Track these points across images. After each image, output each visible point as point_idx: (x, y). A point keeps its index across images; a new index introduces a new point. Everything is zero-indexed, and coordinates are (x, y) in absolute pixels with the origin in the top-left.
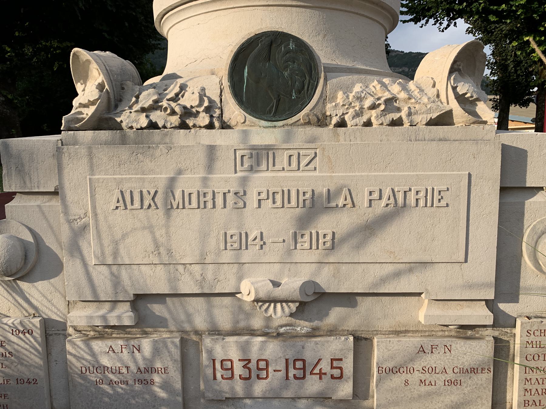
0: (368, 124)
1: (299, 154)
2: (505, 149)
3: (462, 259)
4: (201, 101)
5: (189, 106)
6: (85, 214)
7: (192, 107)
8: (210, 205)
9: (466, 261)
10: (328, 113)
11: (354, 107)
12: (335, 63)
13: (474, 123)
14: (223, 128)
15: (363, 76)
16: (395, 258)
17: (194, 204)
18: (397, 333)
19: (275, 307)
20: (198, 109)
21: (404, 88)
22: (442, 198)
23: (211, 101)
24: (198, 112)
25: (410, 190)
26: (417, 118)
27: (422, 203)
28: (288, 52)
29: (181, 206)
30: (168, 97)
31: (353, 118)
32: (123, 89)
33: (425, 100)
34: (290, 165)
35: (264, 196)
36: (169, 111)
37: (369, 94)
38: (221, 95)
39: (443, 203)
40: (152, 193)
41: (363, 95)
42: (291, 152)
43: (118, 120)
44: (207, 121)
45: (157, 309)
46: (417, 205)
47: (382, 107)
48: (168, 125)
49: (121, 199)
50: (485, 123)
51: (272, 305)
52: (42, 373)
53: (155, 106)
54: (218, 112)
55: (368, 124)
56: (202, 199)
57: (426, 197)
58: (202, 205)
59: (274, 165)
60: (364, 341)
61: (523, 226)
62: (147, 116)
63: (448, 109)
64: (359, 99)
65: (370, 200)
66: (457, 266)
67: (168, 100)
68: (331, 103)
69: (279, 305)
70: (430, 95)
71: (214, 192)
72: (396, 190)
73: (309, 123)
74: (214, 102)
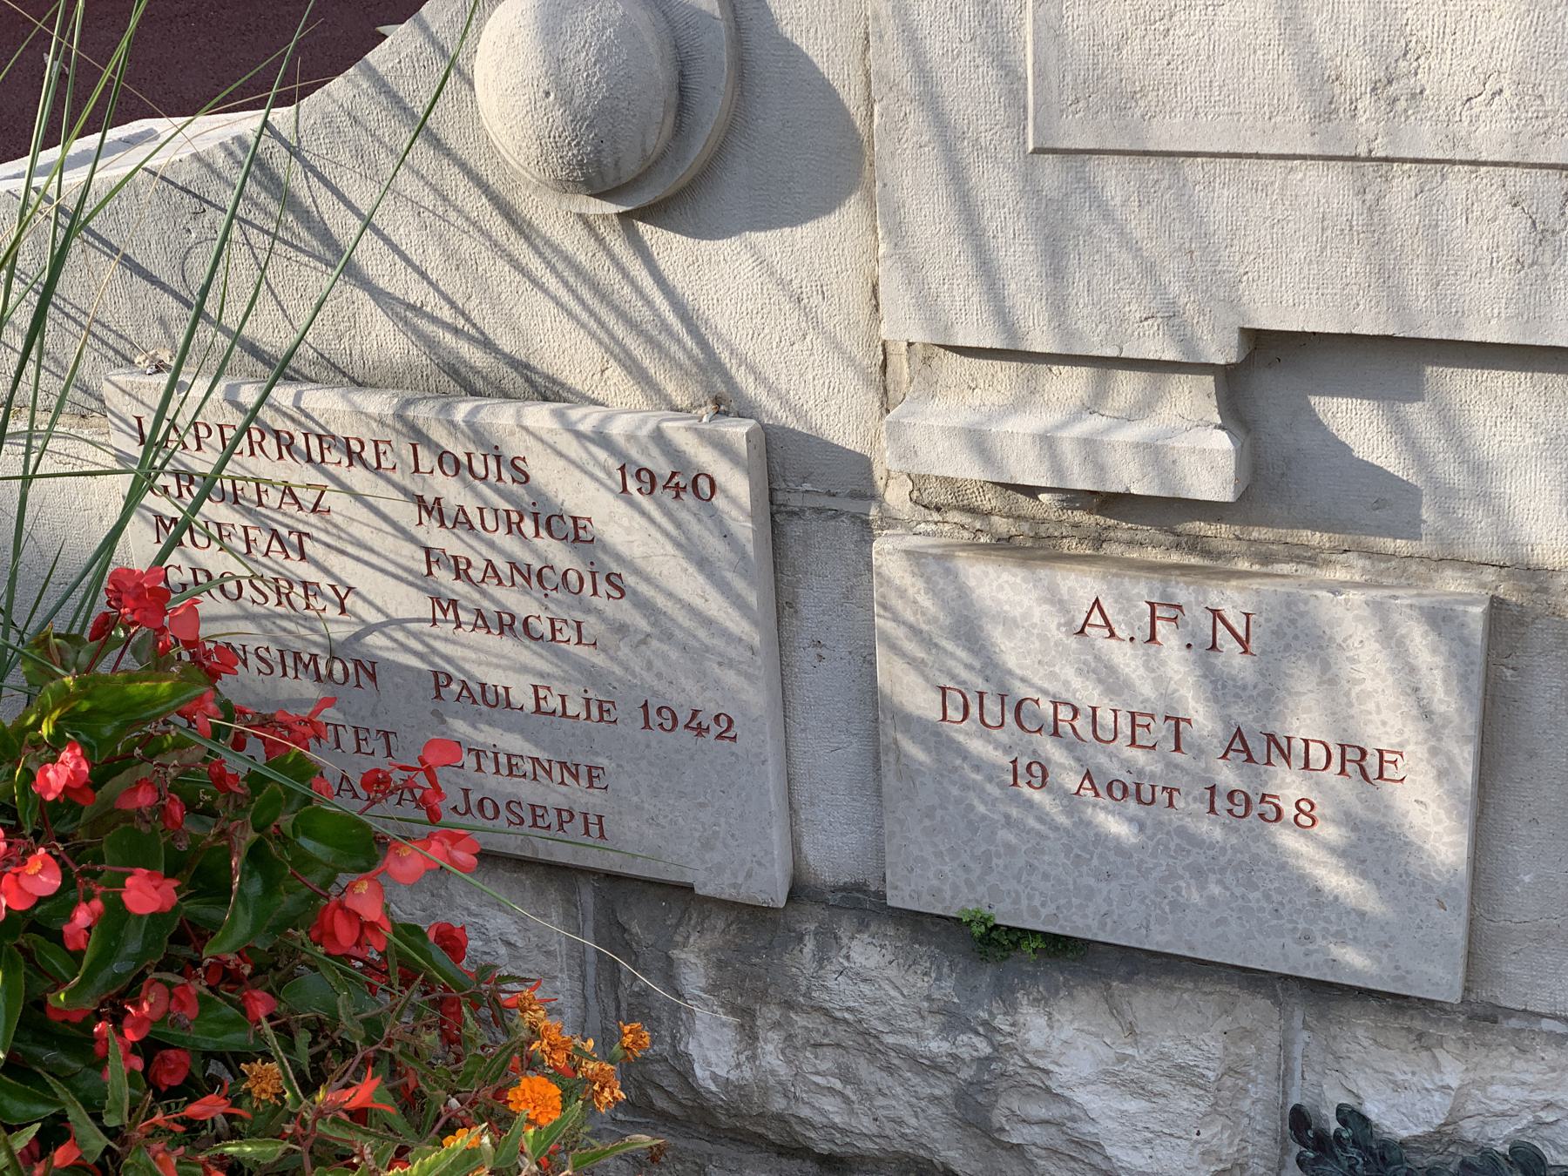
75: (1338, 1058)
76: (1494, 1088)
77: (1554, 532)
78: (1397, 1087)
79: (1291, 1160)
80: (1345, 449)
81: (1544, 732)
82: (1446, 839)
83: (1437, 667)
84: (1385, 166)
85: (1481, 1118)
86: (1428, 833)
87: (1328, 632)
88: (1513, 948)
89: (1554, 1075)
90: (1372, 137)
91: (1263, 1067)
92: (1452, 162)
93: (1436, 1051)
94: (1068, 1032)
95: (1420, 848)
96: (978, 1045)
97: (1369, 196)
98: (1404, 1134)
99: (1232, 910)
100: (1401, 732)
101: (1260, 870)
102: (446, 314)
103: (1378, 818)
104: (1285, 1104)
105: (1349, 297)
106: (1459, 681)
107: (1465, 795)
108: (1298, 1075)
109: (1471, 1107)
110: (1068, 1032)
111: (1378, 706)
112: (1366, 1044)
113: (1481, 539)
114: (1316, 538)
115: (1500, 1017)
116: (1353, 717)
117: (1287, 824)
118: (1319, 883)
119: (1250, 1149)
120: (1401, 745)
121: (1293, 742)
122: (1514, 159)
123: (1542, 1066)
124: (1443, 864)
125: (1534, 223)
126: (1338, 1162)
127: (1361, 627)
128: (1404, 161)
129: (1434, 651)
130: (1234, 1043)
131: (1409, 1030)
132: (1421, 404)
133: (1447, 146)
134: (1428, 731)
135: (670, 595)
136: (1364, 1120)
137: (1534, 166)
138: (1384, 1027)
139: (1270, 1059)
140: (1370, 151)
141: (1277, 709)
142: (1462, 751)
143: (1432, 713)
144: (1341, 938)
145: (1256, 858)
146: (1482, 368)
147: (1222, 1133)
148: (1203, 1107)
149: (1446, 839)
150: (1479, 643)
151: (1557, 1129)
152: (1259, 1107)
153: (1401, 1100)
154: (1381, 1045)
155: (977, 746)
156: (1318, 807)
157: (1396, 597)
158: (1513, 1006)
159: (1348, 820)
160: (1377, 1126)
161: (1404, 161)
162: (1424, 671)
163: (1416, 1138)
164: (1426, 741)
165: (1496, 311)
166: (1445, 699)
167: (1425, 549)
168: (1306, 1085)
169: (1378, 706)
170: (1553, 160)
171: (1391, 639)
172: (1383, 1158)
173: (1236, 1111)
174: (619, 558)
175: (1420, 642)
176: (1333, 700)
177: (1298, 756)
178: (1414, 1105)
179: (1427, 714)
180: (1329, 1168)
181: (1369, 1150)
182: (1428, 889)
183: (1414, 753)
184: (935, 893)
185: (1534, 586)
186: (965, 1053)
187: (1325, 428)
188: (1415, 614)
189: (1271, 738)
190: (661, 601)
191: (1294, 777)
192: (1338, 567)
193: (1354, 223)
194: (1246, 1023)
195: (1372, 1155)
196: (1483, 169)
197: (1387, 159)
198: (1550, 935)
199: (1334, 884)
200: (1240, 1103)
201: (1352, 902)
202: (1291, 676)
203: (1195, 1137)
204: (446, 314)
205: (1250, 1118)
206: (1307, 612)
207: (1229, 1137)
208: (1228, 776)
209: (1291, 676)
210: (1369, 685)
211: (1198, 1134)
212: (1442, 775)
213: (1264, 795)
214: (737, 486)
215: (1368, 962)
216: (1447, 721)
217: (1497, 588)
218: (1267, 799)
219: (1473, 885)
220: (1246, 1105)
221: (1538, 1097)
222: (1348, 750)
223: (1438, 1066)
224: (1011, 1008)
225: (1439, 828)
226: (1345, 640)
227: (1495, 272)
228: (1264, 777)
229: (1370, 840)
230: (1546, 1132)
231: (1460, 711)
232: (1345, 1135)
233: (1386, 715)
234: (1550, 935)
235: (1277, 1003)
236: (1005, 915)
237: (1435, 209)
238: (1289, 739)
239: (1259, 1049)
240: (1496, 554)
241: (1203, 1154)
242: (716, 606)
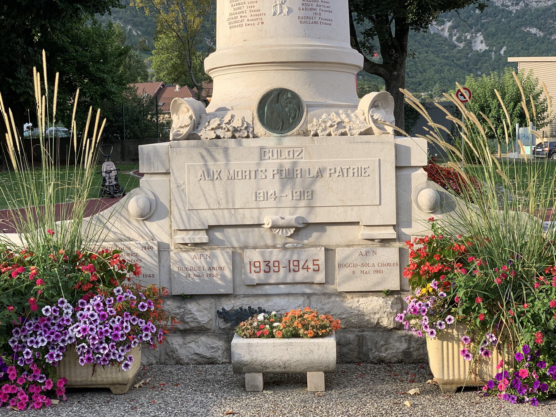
0: (329, 135)
1: (294, 150)
2: (396, 146)
3: (378, 203)
4: (243, 124)
5: (236, 127)
6: (184, 183)
7: (238, 127)
8: (248, 177)
9: (380, 204)
10: (309, 129)
11: (322, 126)
12: (315, 101)
13: (383, 133)
14: (254, 138)
15: (328, 109)
16: (344, 203)
17: (240, 177)
18: (348, 246)
19: (282, 231)
20: (241, 128)
21: (348, 116)
22: (366, 172)
23: (247, 124)
24: (241, 130)
25: (350, 168)
26: (354, 132)
27: (356, 174)
28: (287, 99)
29: (233, 178)
30: (225, 122)
31: (321, 132)
32: (201, 118)
33: (358, 122)
34: (289, 156)
35: (276, 172)
36: (226, 130)
37: (330, 119)
38: (253, 121)
39: (367, 174)
40: (219, 172)
41: (326, 120)
42: (289, 149)
43: (200, 134)
44: (246, 135)
45: (218, 235)
46: (354, 176)
47: (336, 126)
48: (226, 137)
49: (203, 175)
50: (389, 133)
51: (281, 230)
52: (156, 272)
53: (219, 127)
54: (251, 129)
55: (329, 135)
56: (244, 174)
57: (358, 171)
58: (244, 178)
59: (281, 156)
60: (331, 251)
61: (411, 186)
62: (215, 132)
63: (369, 127)
64: (325, 122)
65: (330, 173)
66: (376, 207)
67: (225, 124)
68: (310, 124)
69: (284, 230)
70: (361, 120)
71: (250, 170)
72: (343, 168)
73: (299, 134)
74: (250, 124)
94: (193, 306)
96: (183, 310)
102: (120, 233)
110: (193, 306)
114: (215, 247)
135: (147, 261)
139: (214, 306)
144: (221, 289)
155: (182, 274)
159: (221, 275)
166: (228, 261)
171: (223, 255)
174: (141, 258)
175: (226, 256)
179: (227, 263)
184: (178, 292)
186: (181, 311)
190: (146, 262)
204: (120, 233)
208: (209, 273)
214: (156, 248)
224: (186, 305)
236: (186, 293)
242: (153, 262)
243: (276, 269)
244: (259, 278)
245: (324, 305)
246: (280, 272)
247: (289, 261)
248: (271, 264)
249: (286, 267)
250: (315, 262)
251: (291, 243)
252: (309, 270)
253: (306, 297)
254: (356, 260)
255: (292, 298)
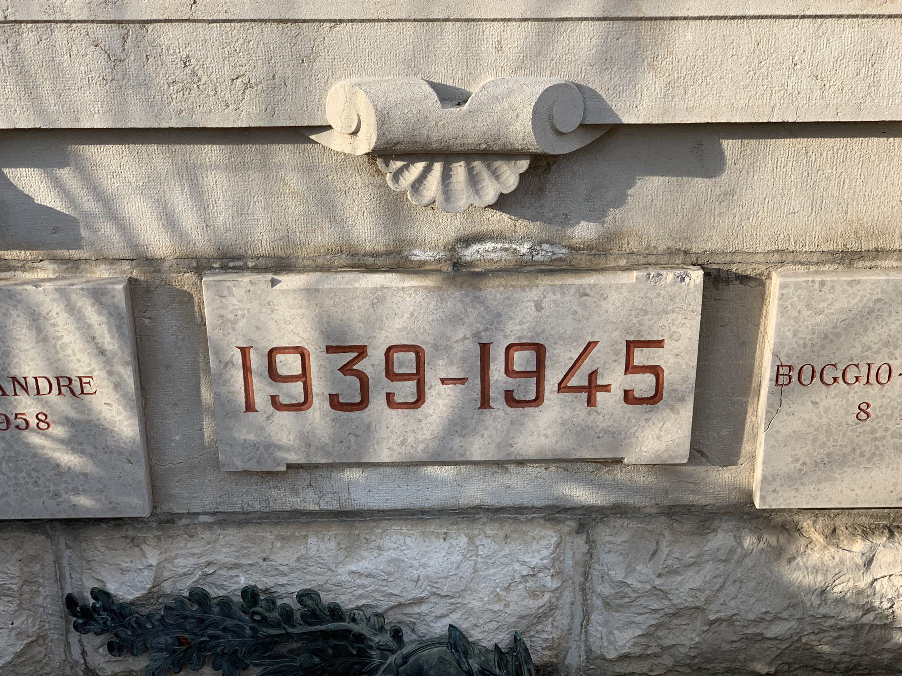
19: (446, 176)
51: (438, 167)
69: (459, 170)
75: (88, 562)
76: (178, 560)
77: (157, 237)
78: (124, 571)
79: (71, 627)
80: (29, 199)
81: (173, 353)
82: (126, 423)
83: (103, 324)
84: (17, 26)
85: (173, 579)
86: (115, 421)
87: (37, 311)
88: (177, 479)
89: (210, 546)
90: (5, 8)
91: (46, 576)
92: (56, 22)
93: (142, 546)
95: (112, 431)
97: (10, 44)
98: (131, 598)
99: (9, 486)
100: (89, 364)
101: (22, 460)
103: (85, 417)
104: (63, 595)
105: (10, 106)
106: (117, 330)
107: (132, 396)
108: (68, 576)
109: (167, 574)
111: (73, 351)
112: (103, 550)
113: (117, 246)
115: (176, 520)
116: (59, 359)
117: (33, 430)
118: (58, 461)
119: (47, 626)
120: (91, 372)
121: (28, 379)
122: (90, 18)
123: (203, 542)
124: (127, 438)
125: (109, 55)
126: (97, 622)
127: (55, 305)
128: (27, 22)
129: (100, 314)
130: (26, 565)
131: (126, 537)
132: (68, 168)
133: (51, 11)
134: (105, 362)
136: (107, 595)
137: (102, 22)
138: (112, 538)
140: (5, 17)
141: (15, 361)
142: (126, 370)
143: (105, 350)
144: (76, 491)
145: (18, 453)
146: (100, 144)
147: (27, 620)
148: (13, 607)
149: (126, 423)
150: (124, 306)
151: (216, 576)
152: (48, 600)
153: (127, 579)
154: (110, 549)
156: (49, 417)
157: (72, 285)
158: (182, 512)
159: (67, 421)
160: (115, 597)
161: (27, 22)
162: (96, 327)
163: (138, 599)
164: (105, 367)
165: (96, 109)
166: (110, 342)
167: (86, 255)
168: (73, 581)
169: (73, 351)
170: (112, 18)
171: (71, 309)
172: (121, 613)
173: (34, 606)
176: (47, 351)
177: (32, 387)
178: (134, 580)
179: (102, 352)
180: (91, 627)
181: (112, 611)
182: (120, 453)
183: (99, 375)
185: (152, 269)
187: (15, 187)
188: (85, 293)
189: (14, 379)
191: (32, 401)
192: (39, 270)
193: (4, 61)
194: (31, 552)
195: (116, 614)
196: (74, 25)
197: (16, 21)
198: (195, 467)
199: (66, 460)
200: (36, 600)
201: (78, 469)
202: (19, 340)
203: (11, 626)
205: (44, 608)
206: (22, 300)
207: (32, 621)
209: (19, 340)
210: (66, 339)
211: (12, 624)
212: (117, 386)
213: (16, 415)
215: (94, 502)
216: (115, 354)
217: (132, 273)
218: (19, 416)
219: (148, 447)
220: (40, 600)
221: (203, 560)
222: (61, 379)
223: (144, 555)
225: (119, 418)
226: (47, 314)
227: (92, 86)
228: (14, 403)
229: (83, 431)
230: (210, 579)
231: (120, 347)
232: (98, 606)
233: (79, 355)
234: (195, 467)
235: (49, 537)
237: (50, 50)
238: (25, 378)
239: (42, 566)
240: (126, 253)
241: (17, 635)
243: (406, 390)
244: (306, 441)
245: (673, 572)
246: (426, 407)
247: (484, 348)
248: (372, 365)
249: (461, 380)
250: (641, 357)
251: (498, 237)
252: (600, 395)
253: (573, 524)
254: (887, 344)
255: (491, 529)
